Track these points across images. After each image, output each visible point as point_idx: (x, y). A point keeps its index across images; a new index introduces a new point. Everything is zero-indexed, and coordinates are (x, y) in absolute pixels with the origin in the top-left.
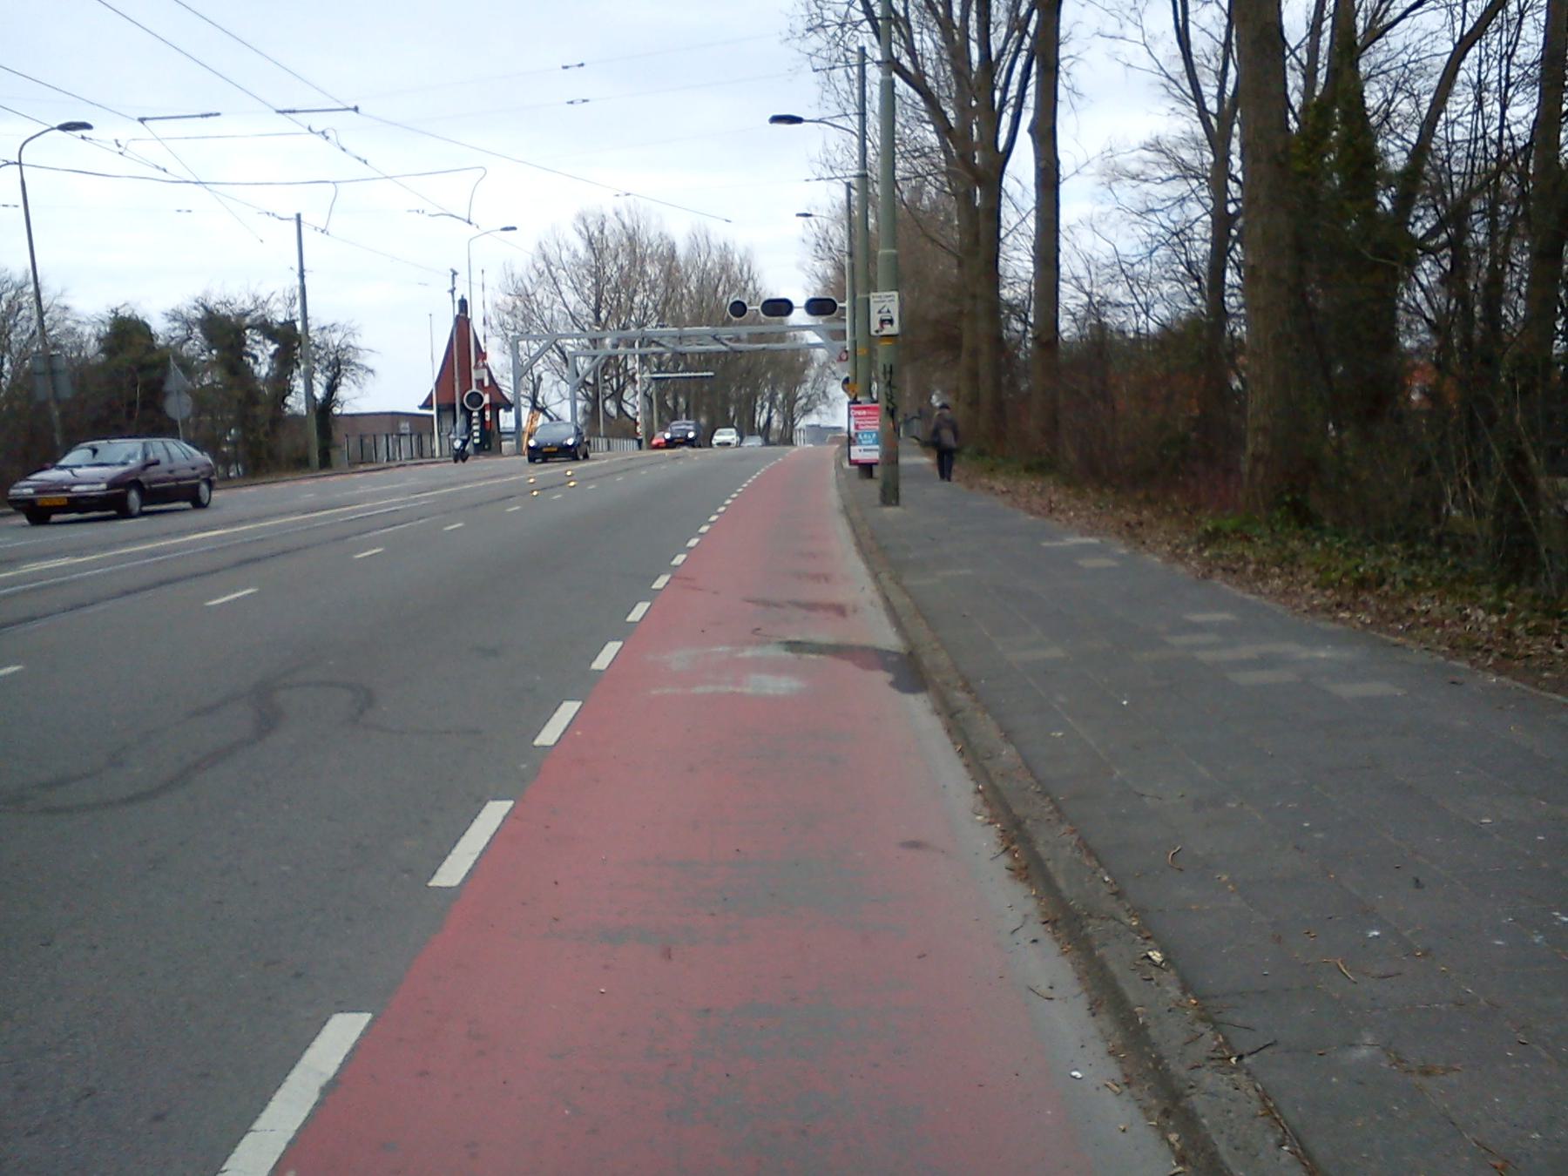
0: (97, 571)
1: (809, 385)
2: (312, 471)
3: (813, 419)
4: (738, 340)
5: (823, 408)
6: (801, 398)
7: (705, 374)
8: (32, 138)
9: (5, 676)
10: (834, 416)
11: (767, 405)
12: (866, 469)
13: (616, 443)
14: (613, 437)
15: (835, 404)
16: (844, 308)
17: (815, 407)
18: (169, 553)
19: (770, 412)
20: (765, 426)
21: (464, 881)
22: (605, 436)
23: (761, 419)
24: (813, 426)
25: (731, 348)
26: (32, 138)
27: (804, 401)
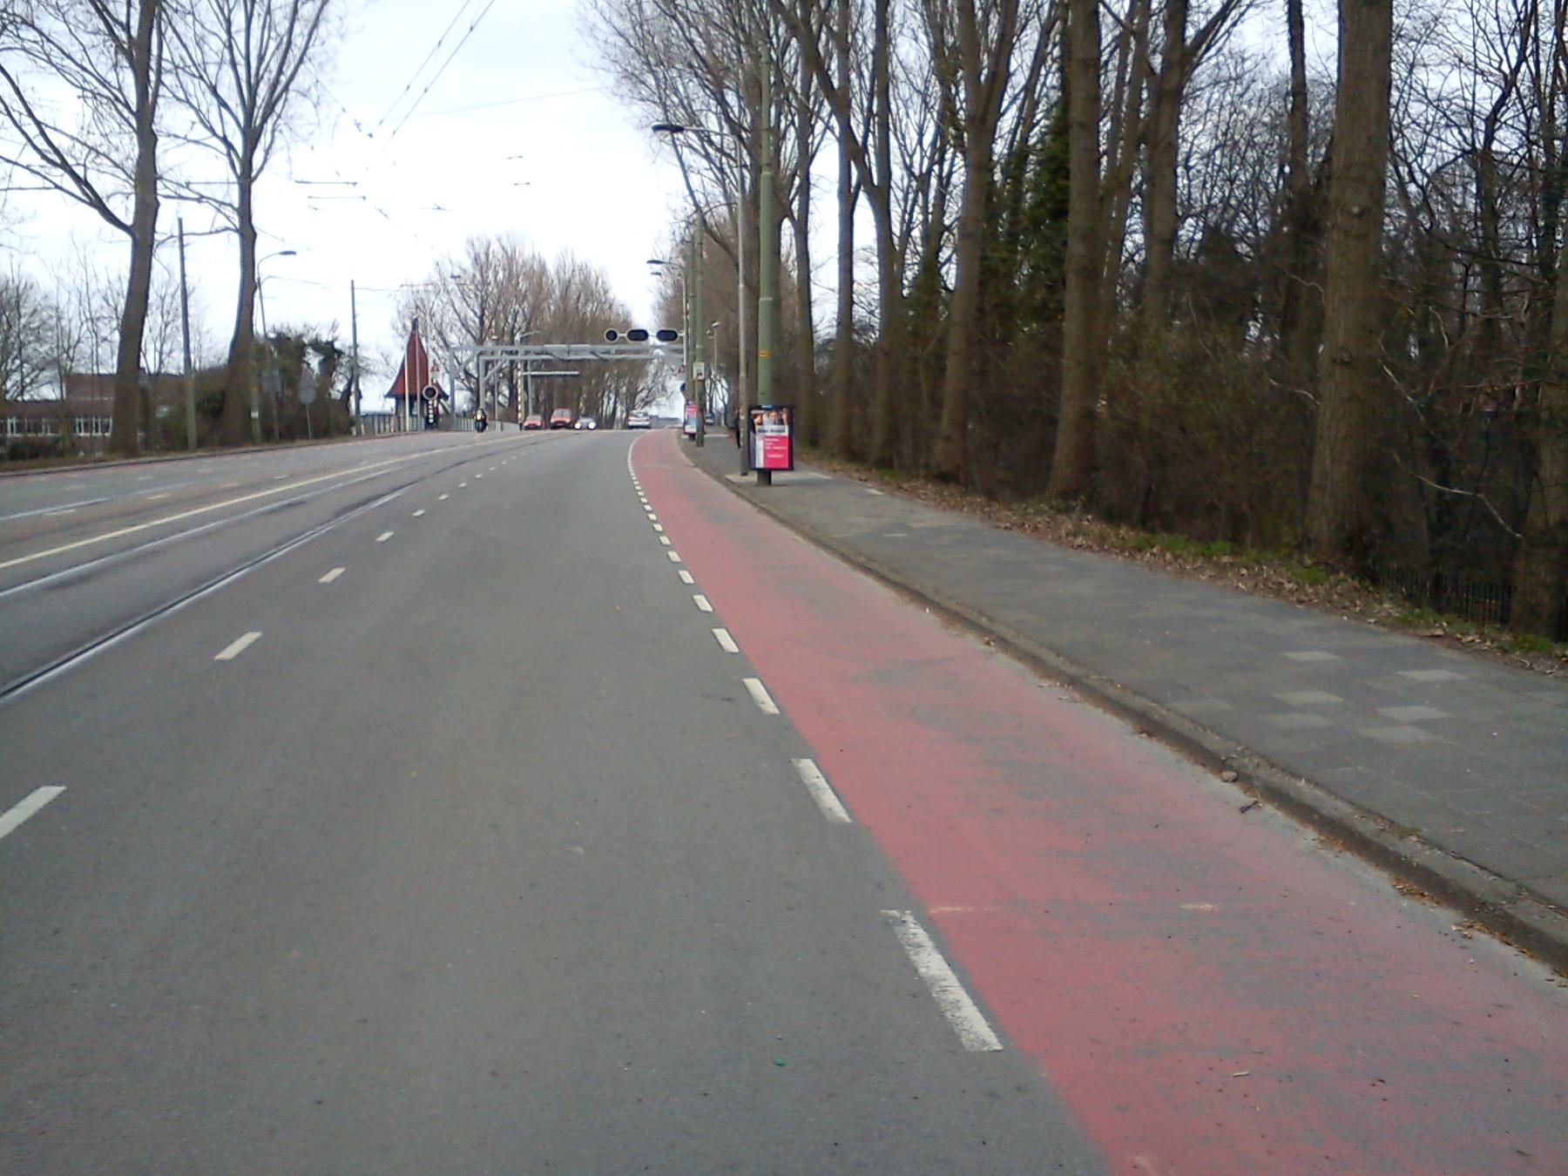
2: (254, 444)
4: (608, 352)
5: (662, 400)
6: (641, 391)
7: (573, 373)
8: (199, 235)
10: (672, 408)
11: (613, 397)
12: (692, 436)
13: (506, 424)
14: (505, 421)
16: (682, 337)
19: (615, 403)
22: (499, 420)
23: (607, 408)
25: (602, 359)
26: (199, 235)
27: (643, 394)
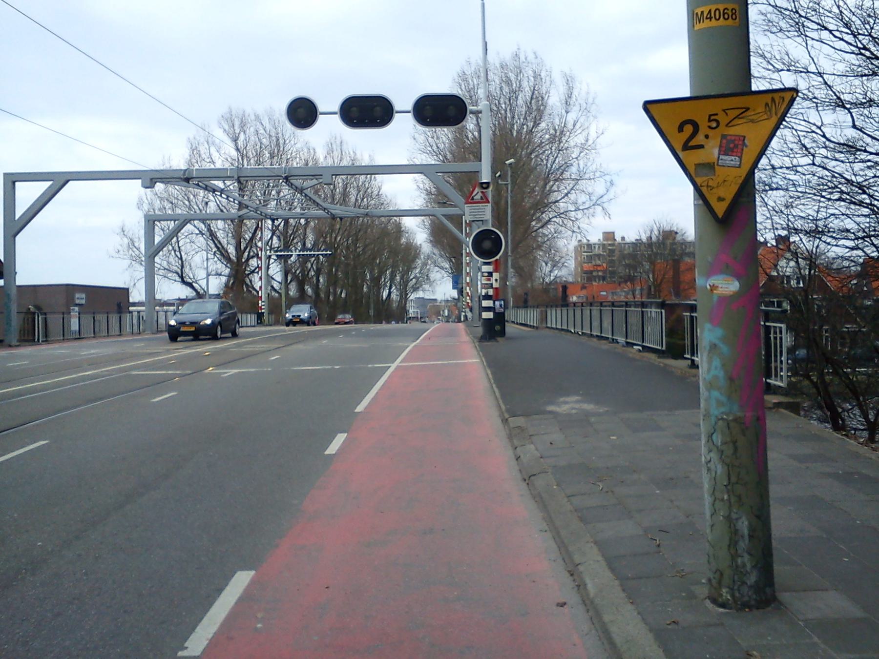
0: (72, 386)
1: (418, 270)
3: (420, 294)
5: (426, 287)
6: (412, 280)
9: (2, 462)
15: (434, 284)
17: (421, 285)
18: (63, 386)
19: (390, 288)
20: (387, 298)
21: (203, 653)
24: (419, 298)
